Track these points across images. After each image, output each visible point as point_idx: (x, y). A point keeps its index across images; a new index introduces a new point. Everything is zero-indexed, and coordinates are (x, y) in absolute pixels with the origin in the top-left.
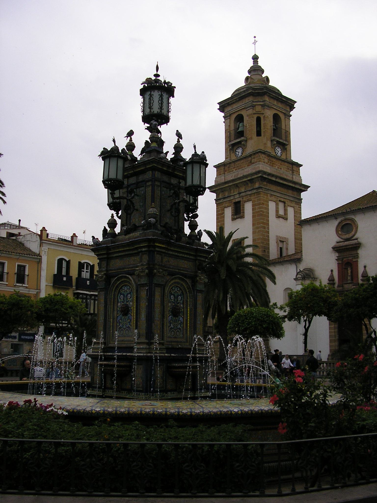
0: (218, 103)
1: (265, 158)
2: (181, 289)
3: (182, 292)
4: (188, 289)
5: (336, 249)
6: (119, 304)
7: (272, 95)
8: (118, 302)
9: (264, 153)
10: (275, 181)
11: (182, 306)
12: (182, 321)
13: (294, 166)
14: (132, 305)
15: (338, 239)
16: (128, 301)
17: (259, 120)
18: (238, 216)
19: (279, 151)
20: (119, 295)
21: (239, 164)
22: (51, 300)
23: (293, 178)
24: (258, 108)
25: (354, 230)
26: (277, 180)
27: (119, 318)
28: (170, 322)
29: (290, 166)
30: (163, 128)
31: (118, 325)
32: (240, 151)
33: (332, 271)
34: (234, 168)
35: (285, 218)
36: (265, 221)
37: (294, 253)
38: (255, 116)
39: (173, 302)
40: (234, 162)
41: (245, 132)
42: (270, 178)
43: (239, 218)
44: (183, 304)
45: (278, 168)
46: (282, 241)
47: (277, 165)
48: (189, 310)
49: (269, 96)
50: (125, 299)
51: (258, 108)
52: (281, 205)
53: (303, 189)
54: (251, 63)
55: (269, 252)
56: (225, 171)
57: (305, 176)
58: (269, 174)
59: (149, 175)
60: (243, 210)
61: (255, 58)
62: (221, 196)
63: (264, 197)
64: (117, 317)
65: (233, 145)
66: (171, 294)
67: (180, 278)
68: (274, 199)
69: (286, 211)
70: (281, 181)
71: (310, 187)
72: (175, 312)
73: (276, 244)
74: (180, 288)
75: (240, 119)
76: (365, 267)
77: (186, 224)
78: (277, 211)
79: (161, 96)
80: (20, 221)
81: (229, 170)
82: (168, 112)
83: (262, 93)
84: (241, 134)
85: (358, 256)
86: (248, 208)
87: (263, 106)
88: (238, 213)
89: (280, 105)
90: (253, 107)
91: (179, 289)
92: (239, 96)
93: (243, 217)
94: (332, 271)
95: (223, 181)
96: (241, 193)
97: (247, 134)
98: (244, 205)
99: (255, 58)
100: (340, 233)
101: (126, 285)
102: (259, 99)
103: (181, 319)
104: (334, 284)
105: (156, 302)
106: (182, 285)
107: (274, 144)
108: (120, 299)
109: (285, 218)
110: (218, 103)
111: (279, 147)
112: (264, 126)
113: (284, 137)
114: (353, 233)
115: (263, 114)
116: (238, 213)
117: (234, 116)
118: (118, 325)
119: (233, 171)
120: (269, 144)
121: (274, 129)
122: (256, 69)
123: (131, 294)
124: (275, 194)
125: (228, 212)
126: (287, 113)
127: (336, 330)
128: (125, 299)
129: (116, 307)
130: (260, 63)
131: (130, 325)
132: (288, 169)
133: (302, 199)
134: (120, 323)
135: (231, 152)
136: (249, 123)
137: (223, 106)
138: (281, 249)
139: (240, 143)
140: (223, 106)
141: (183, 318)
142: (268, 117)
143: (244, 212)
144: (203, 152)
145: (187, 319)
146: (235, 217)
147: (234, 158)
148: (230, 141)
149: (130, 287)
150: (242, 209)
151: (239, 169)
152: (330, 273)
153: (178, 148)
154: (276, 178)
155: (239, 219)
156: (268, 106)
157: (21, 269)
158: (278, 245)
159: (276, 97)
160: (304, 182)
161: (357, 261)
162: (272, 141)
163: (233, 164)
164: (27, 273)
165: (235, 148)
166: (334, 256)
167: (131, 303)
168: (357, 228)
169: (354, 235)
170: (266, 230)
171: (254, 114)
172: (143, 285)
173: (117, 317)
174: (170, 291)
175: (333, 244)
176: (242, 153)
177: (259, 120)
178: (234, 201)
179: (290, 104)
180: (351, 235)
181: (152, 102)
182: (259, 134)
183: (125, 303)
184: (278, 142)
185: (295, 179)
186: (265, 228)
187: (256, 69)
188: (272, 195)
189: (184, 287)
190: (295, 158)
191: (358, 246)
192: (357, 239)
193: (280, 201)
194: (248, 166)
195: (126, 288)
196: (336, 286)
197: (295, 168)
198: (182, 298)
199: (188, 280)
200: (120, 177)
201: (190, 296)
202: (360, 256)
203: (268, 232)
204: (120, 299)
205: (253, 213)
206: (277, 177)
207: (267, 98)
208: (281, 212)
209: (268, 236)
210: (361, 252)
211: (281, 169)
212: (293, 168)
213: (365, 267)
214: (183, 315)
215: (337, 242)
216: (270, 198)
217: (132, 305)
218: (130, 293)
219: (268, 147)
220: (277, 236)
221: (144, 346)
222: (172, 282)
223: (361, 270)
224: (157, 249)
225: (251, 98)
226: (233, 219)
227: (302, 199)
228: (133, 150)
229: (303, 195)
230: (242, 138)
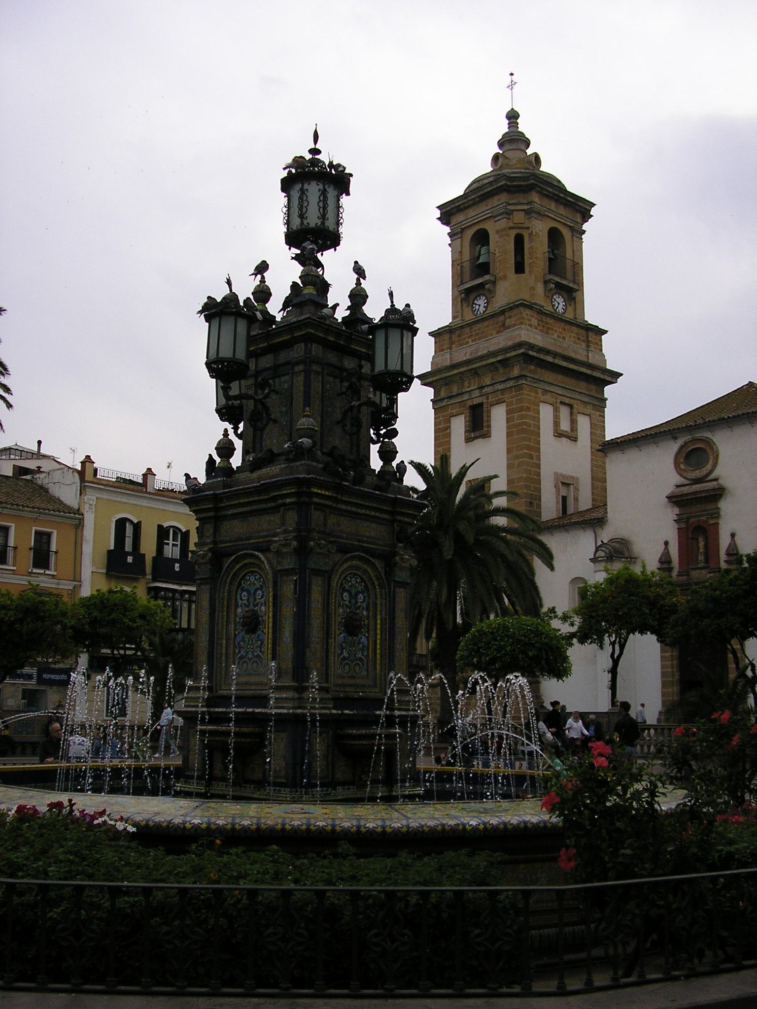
1: (532, 316)
2: (363, 580)
4: (378, 579)
5: (675, 499)
6: (239, 610)
7: (546, 190)
8: (237, 606)
9: (530, 307)
11: (365, 613)
12: (366, 643)
13: (590, 334)
14: (266, 612)
15: (679, 480)
17: (519, 241)
18: (477, 433)
19: (560, 303)
20: (239, 592)
21: (479, 329)
23: (588, 356)
24: (519, 217)
25: (711, 462)
26: (556, 361)
27: (239, 639)
28: (341, 645)
29: (583, 332)
30: (326, 257)
31: (237, 651)
32: (481, 302)
33: (666, 543)
34: (469, 337)
35: (573, 437)
36: (532, 444)
38: (513, 233)
39: (347, 607)
40: (469, 325)
41: (491, 265)
42: (542, 356)
43: (480, 437)
44: (368, 609)
45: (558, 337)
46: (565, 483)
47: (556, 331)
48: (379, 621)
49: (538, 192)
50: (251, 599)
51: (519, 217)
52: (564, 412)
53: (609, 379)
54: (503, 127)
55: (539, 506)
56: (452, 343)
57: (613, 353)
58: (541, 350)
59: (298, 351)
60: (489, 421)
61: (513, 117)
62: (443, 394)
63: (531, 396)
64: (236, 635)
65: (469, 292)
66: (344, 590)
67: (361, 558)
68: (551, 400)
69: (573, 423)
71: (622, 375)
72: (352, 627)
73: (554, 490)
74: (361, 578)
75: (482, 238)
76: (733, 535)
77: (374, 449)
78: (556, 424)
79: (324, 193)
80: (40, 442)
81: (459, 341)
82: (338, 224)
83: (527, 186)
84: (483, 269)
85: (718, 513)
86: (498, 417)
87: (527, 212)
88: (478, 427)
89: (562, 210)
91: (359, 580)
93: (487, 435)
94: (666, 543)
95: (448, 363)
96: (483, 387)
97: (496, 269)
98: (489, 412)
99: (513, 117)
100: (682, 466)
101: (252, 572)
102: (521, 198)
103: (364, 639)
104: (670, 570)
105: (313, 605)
106: (365, 571)
107: (551, 290)
108: (241, 599)
109: (573, 437)
110: (438, 207)
111: (560, 294)
112: (530, 254)
113: (569, 275)
114: (709, 467)
115: (528, 228)
116: (478, 427)
117: (470, 233)
118: (237, 651)
119: (468, 342)
120: (540, 289)
121: (550, 260)
122: (514, 139)
124: (552, 389)
125: (459, 425)
126: (576, 227)
128: (251, 599)
129: (232, 616)
130: (523, 126)
131: (261, 651)
132: (579, 339)
133: (606, 399)
134: (240, 648)
137: (449, 213)
138: (564, 499)
139: (481, 286)
140: (449, 213)
141: (367, 638)
142: (537, 234)
143: (489, 426)
144: (408, 305)
145: (376, 641)
146: (473, 435)
147: (469, 317)
149: (261, 577)
150: (485, 418)
151: (479, 339)
152: (663, 547)
153: (358, 297)
154: (555, 358)
155: (481, 440)
156: (539, 213)
158: (558, 491)
159: (555, 194)
160: (611, 365)
161: (717, 524)
162: (546, 282)
163: (467, 330)
165: (472, 297)
166: (672, 513)
167: (263, 608)
169: (711, 472)
170: (535, 461)
171: (510, 228)
172: (288, 572)
173: (236, 635)
174: (342, 584)
175: (670, 489)
176: (486, 308)
177: (519, 241)
178: (470, 403)
179: (582, 209)
180: (704, 471)
181: (305, 204)
182: (520, 268)
183: (251, 607)
184: (559, 286)
185: (593, 359)
186: (531, 457)
187: (514, 139)
188: (545, 392)
189: (369, 576)
190: (591, 317)
191: (718, 493)
193: (562, 403)
194: (498, 332)
195: (252, 579)
196: (675, 573)
197: (592, 337)
198: (364, 597)
199: (377, 563)
200: (241, 355)
202: (722, 513)
203: (538, 466)
204: (241, 599)
205: (508, 428)
206: (555, 355)
207: (535, 197)
208: (565, 426)
209: (539, 474)
210: (724, 505)
211: (564, 338)
212: (588, 337)
213: (733, 535)
214: (368, 632)
215: (677, 486)
216: (543, 398)
217: (266, 612)
218: (261, 588)
220: (556, 474)
222: (345, 566)
223: (724, 542)
224: (315, 500)
225: (504, 198)
226: (468, 440)
227: (606, 399)
230: (487, 277)
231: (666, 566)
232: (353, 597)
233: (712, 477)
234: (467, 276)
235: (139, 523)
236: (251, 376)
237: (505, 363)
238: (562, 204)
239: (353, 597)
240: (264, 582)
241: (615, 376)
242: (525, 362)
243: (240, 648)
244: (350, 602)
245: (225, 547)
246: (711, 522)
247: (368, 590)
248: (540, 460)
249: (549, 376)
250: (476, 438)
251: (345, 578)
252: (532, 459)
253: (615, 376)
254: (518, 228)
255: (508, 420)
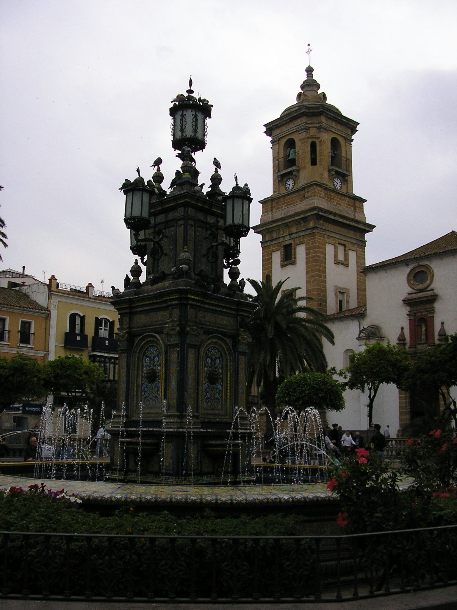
0: (264, 125)
2: (219, 351)
3: (221, 355)
4: (228, 350)
5: (407, 302)
6: (144, 369)
8: (143, 366)
9: (320, 185)
10: (334, 220)
11: (220, 371)
12: (221, 388)
13: (356, 202)
14: (160, 370)
15: (410, 290)
16: (155, 366)
17: (313, 146)
18: (288, 262)
19: (338, 183)
20: (145, 358)
22: (61, 364)
23: (355, 215)
24: (313, 131)
25: (429, 279)
26: (336, 218)
27: (144, 386)
28: (206, 390)
29: (352, 201)
30: (197, 156)
31: (143, 394)
32: (291, 183)
33: (402, 328)
34: (283, 204)
35: (346, 264)
36: (321, 269)
37: (356, 306)
38: (310, 141)
39: (210, 367)
40: (283, 196)
42: (327, 215)
43: (289, 264)
44: (222, 368)
45: (337, 203)
46: (341, 292)
47: (336, 200)
48: (229, 376)
50: (152, 362)
51: (313, 131)
52: (341, 249)
53: (368, 229)
54: (304, 77)
55: (325, 306)
57: (370, 214)
58: (326, 212)
59: (180, 212)
60: (295, 254)
61: (309, 71)
62: (267, 238)
63: (320, 239)
64: (142, 384)
65: (283, 176)
66: (208, 357)
68: (333, 242)
69: (346, 255)
70: (341, 220)
71: (375, 226)
72: (213, 379)
73: (334, 296)
74: (218, 349)
75: (291, 144)
76: (442, 324)
77: (226, 271)
78: (336, 256)
79: (195, 116)
80: (24, 267)
81: (277, 206)
82: (204, 135)
83: (318, 112)
84: (292, 162)
86: (301, 252)
87: (319, 128)
88: (288, 258)
89: (339, 127)
90: (307, 129)
91: (216, 351)
92: (290, 116)
93: (294, 263)
94: (402, 328)
95: (271, 220)
97: (300, 163)
98: (295, 249)
99: (309, 71)
100: (412, 282)
101: (152, 346)
102: (314, 120)
103: (220, 386)
104: (405, 344)
105: (189, 366)
106: (220, 345)
108: (146, 362)
109: (346, 264)
110: (264, 125)
111: (338, 178)
112: (320, 153)
114: (428, 282)
115: (319, 138)
116: (288, 258)
117: (284, 141)
118: (143, 394)
119: (283, 207)
120: (326, 174)
122: (310, 84)
123: (159, 356)
125: (277, 257)
126: (348, 137)
127: (407, 400)
128: (152, 362)
129: (140, 373)
130: (316, 76)
131: (157, 394)
133: (366, 241)
135: (281, 184)
136: (302, 150)
137: (271, 129)
138: (341, 302)
139: (290, 173)
140: (271, 129)
141: (222, 386)
144: (246, 185)
145: (227, 387)
147: (283, 191)
148: (279, 171)
149: (158, 349)
151: (289, 205)
152: (400, 331)
153: (216, 180)
154: (335, 216)
155: (290, 266)
156: (325, 129)
157: (26, 326)
159: (335, 117)
160: (369, 221)
161: (433, 317)
162: (329, 171)
163: (282, 199)
164: (32, 331)
165: (285, 179)
166: (405, 310)
168: (433, 276)
170: (323, 279)
172: (174, 346)
173: (142, 384)
174: (206, 353)
175: (404, 296)
176: (293, 186)
177: (313, 146)
178: (283, 244)
179: (351, 126)
180: (425, 285)
181: (184, 123)
182: (314, 162)
183: (152, 367)
184: (337, 173)
185: (358, 217)
186: (321, 276)
187: (310, 84)
188: (329, 237)
189: (223, 348)
190: (357, 191)
191: (434, 298)
192: (432, 290)
193: (339, 244)
194: (301, 201)
195: (152, 350)
196: (407, 347)
197: (357, 203)
198: (220, 361)
199: (228, 340)
200: (145, 214)
201: (230, 359)
202: (436, 310)
203: (325, 282)
204: (146, 362)
205: (307, 258)
206: (335, 214)
207: (323, 119)
208: (341, 257)
209: (325, 287)
210: (437, 305)
211: (340, 204)
212: (355, 204)
213: (442, 324)
214: (222, 382)
215: (409, 294)
216: (328, 241)
217: (160, 370)
218: (158, 355)
219: (325, 179)
220: (335, 286)
221: (175, 420)
222: (208, 342)
223: (437, 328)
224: (190, 302)
226: (283, 266)
227: (366, 241)
228: (161, 182)
229: (367, 236)
230: (294, 168)
231: (402, 342)
232: (213, 361)
233: (430, 288)
234: (282, 167)
235: (84, 316)
236: (152, 227)
237: (305, 219)
238: (339, 123)
239: (213, 361)
240: (159, 352)
241: (371, 227)
242: (317, 219)
243: (145, 391)
244: (211, 364)
245: (136, 331)
246: (429, 315)
247: (222, 356)
248: (326, 278)
249: (331, 227)
250: (287, 265)
251: (208, 350)
252: (321, 277)
253: (371, 227)
254: (312, 138)
255: (307, 254)
